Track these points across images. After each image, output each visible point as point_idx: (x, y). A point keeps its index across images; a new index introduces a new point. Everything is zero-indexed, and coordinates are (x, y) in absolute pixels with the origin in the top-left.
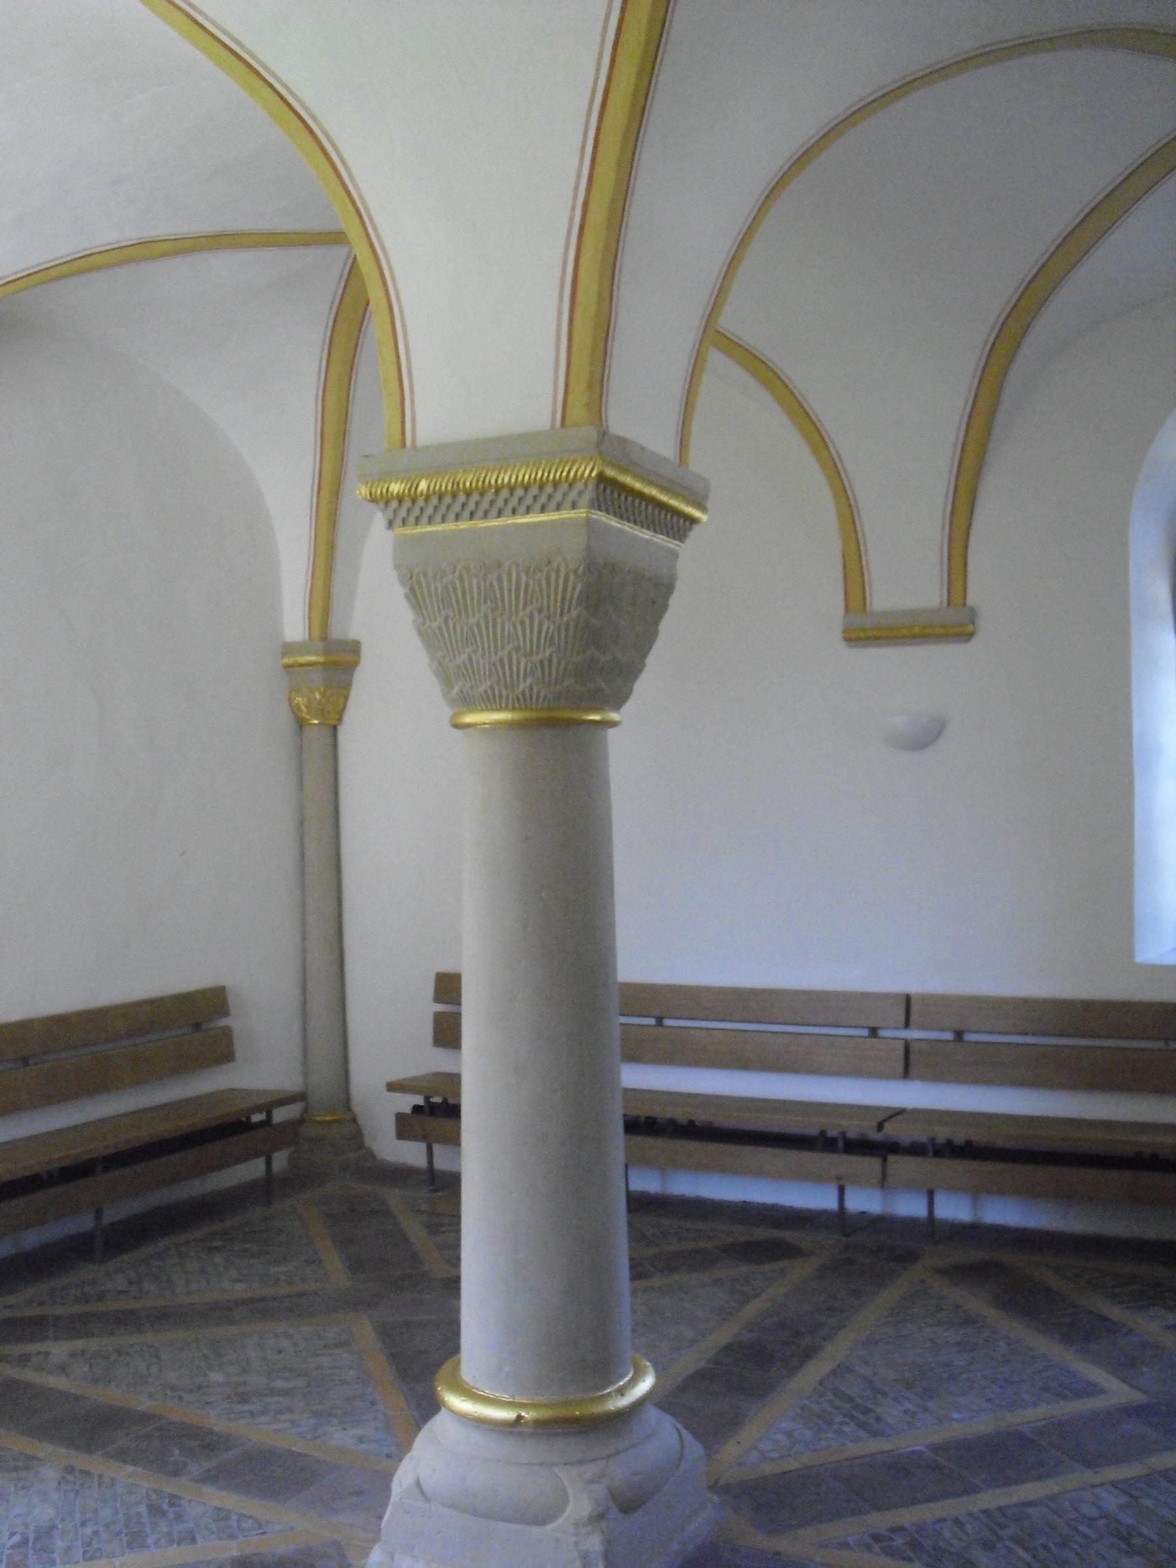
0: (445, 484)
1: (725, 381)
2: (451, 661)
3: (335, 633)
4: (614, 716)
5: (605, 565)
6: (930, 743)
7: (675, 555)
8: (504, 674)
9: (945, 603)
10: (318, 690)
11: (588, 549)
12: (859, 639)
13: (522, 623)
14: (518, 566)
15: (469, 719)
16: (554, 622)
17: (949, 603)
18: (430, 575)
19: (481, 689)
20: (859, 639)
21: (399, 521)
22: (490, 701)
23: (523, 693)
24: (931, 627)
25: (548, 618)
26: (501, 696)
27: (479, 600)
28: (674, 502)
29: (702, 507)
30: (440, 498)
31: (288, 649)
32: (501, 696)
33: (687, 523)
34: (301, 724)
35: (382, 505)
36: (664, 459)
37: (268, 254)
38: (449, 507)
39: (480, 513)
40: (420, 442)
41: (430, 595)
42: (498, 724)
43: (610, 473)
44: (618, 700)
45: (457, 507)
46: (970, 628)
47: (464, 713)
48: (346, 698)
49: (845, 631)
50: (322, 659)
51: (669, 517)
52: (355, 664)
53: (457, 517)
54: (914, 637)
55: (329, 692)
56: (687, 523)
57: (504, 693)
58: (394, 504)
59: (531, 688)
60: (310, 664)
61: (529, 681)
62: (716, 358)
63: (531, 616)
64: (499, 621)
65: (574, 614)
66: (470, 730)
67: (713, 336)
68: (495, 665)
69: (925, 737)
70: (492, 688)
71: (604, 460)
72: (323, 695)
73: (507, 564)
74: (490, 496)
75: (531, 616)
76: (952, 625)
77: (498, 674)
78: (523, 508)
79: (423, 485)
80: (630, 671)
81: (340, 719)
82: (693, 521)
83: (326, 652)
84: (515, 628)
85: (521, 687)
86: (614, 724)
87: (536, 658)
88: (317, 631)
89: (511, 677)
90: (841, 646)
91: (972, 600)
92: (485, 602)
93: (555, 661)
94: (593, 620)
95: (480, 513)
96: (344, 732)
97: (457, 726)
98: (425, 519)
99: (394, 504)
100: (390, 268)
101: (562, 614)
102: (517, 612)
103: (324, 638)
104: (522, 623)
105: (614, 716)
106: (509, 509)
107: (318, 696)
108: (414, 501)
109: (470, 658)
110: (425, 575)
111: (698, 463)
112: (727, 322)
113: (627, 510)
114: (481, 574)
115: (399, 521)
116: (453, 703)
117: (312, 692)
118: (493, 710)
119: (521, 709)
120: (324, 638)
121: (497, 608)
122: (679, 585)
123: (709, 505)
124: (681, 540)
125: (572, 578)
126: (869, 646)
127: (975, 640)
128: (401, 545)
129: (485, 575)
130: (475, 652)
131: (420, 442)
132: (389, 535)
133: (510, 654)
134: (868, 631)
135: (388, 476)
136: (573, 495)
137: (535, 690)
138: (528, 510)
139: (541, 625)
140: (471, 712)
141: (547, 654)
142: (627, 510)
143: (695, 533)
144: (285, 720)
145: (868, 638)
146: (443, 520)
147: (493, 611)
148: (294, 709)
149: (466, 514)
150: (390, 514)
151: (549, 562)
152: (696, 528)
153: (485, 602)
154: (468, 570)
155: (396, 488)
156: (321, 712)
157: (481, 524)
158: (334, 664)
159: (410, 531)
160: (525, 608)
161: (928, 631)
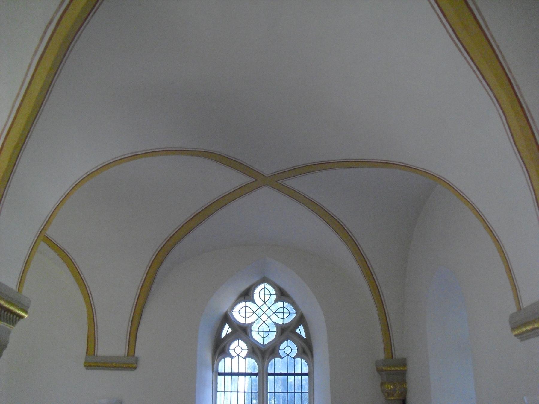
1: (46, 257)
7: (10, 332)
9: (126, 355)
28: (12, 308)
29: (26, 312)
33: (18, 318)
36: (12, 289)
46: (135, 365)
49: (85, 362)
51: (12, 316)
56: (18, 318)
62: (43, 246)
67: (43, 237)
76: (128, 363)
82: (21, 317)
100: (495, 41)
111: (25, 292)
112: (50, 232)
113: (7, 318)
122: (9, 345)
123: (29, 311)
124: (13, 325)
134: (95, 363)
142: (7, 318)
143: (21, 323)
145: (94, 366)
152: (21, 320)
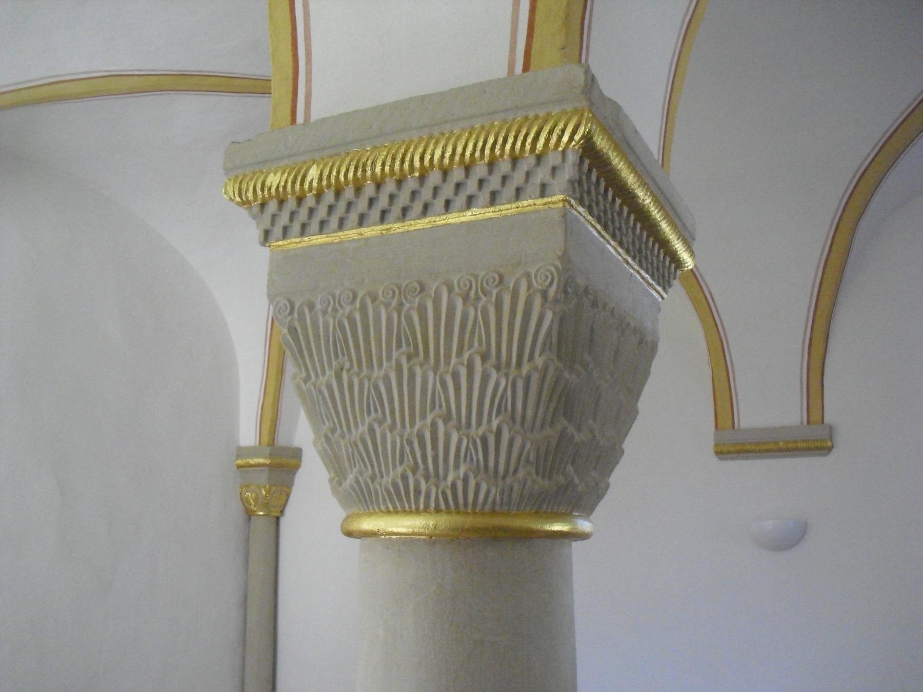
0: (346, 172)
2: (343, 436)
3: (281, 441)
4: (584, 525)
5: (586, 291)
6: (793, 546)
8: (424, 456)
10: (265, 487)
11: (565, 257)
12: (729, 452)
13: (456, 376)
14: (450, 290)
15: (368, 524)
16: (507, 375)
17: (808, 422)
18: (319, 307)
19: (387, 480)
20: (729, 452)
21: (277, 231)
22: (401, 500)
23: (454, 486)
24: (795, 442)
25: (498, 368)
26: (418, 492)
27: (389, 342)
30: (338, 194)
31: (242, 452)
32: (418, 492)
34: (249, 514)
35: (256, 210)
37: (227, 101)
38: (349, 205)
39: (396, 211)
40: (316, 114)
41: (317, 336)
42: (407, 541)
43: (601, 142)
44: (581, 500)
45: (362, 205)
46: (829, 444)
47: (359, 516)
48: (288, 495)
49: (716, 445)
50: (268, 462)
52: (296, 467)
53: (362, 221)
54: (780, 450)
55: (274, 489)
57: (423, 487)
58: (273, 206)
59: (466, 480)
60: (259, 465)
61: (463, 469)
63: (470, 368)
64: (418, 372)
65: (539, 361)
66: (369, 540)
68: (410, 443)
69: (790, 539)
70: (404, 478)
71: (595, 119)
72: (268, 492)
73: (433, 287)
74: (411, 184)
75: (470, 368)
76: (811, 440)
77: (415, 458)
78: (461, 200)
79: (313, 173)
80: (606, 457)
81: (282, 512)
83: (271, 455)
84: (444, 384)
85: (450, 478)
86: (584, 536)
87: (476, 432)
88: (265, 439)
89: (435, 459)
90: (714, 459)
91: (827, 419)
92: (399, 346)
93: (506, 436)
94: (566, 375)
95: (396, 211)
96: (284, 522)
97: (349, 534)
98: (315, 225)
99: (273, 206)
101: (519, 364)
102: (448, 357)
103: (272, 443)
104: (456, 376)
105: (584, 525)
106: (439, 203)
107: (264, 493)
108: (300, 200)
109: (372, 430)
110: (311, 307)
114: (394, 303)
115: (277, 231)
116: (345, 500)
117: (259, 488)
118: (406, 512)
119: (448, 511)
120: (272, 443)
121: (417, 354)
125: (537, 302)
126: (737, 458)
127: (834, 453)
128: (280, 267)
129: (401, 304)
130: (381, 423)
131: (316, 114)
132: (264, 253)
133: (434, 425)
134: (736, 446)
135: (266, 164)
136: (541, 175)
137: (472, 483)
138: (470, 202)
139: (485, 378)
140: (371, 514)
141: (495, 424)
144: (236, 508)
146: (341, 225)
147: (409, 358)
148: (244, 501)
149: (375, 214)
150: (267, 223)
151: (501, 278)
153: (399, 346)
154: (374, 299)
155: (274, 180)
156: (266, 506)
157: (397, 228)
158: (283, 466)
159: (294, 243)
160: (460, 353)
161: (790, 446)
